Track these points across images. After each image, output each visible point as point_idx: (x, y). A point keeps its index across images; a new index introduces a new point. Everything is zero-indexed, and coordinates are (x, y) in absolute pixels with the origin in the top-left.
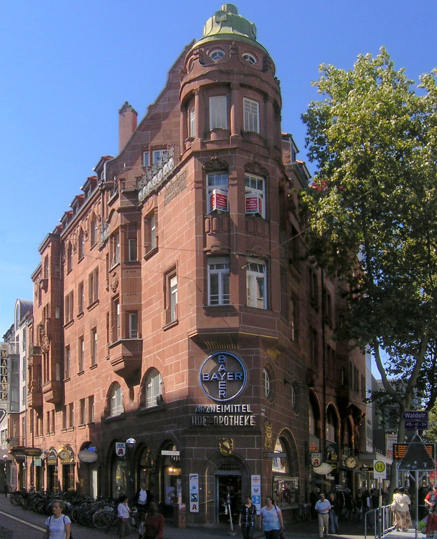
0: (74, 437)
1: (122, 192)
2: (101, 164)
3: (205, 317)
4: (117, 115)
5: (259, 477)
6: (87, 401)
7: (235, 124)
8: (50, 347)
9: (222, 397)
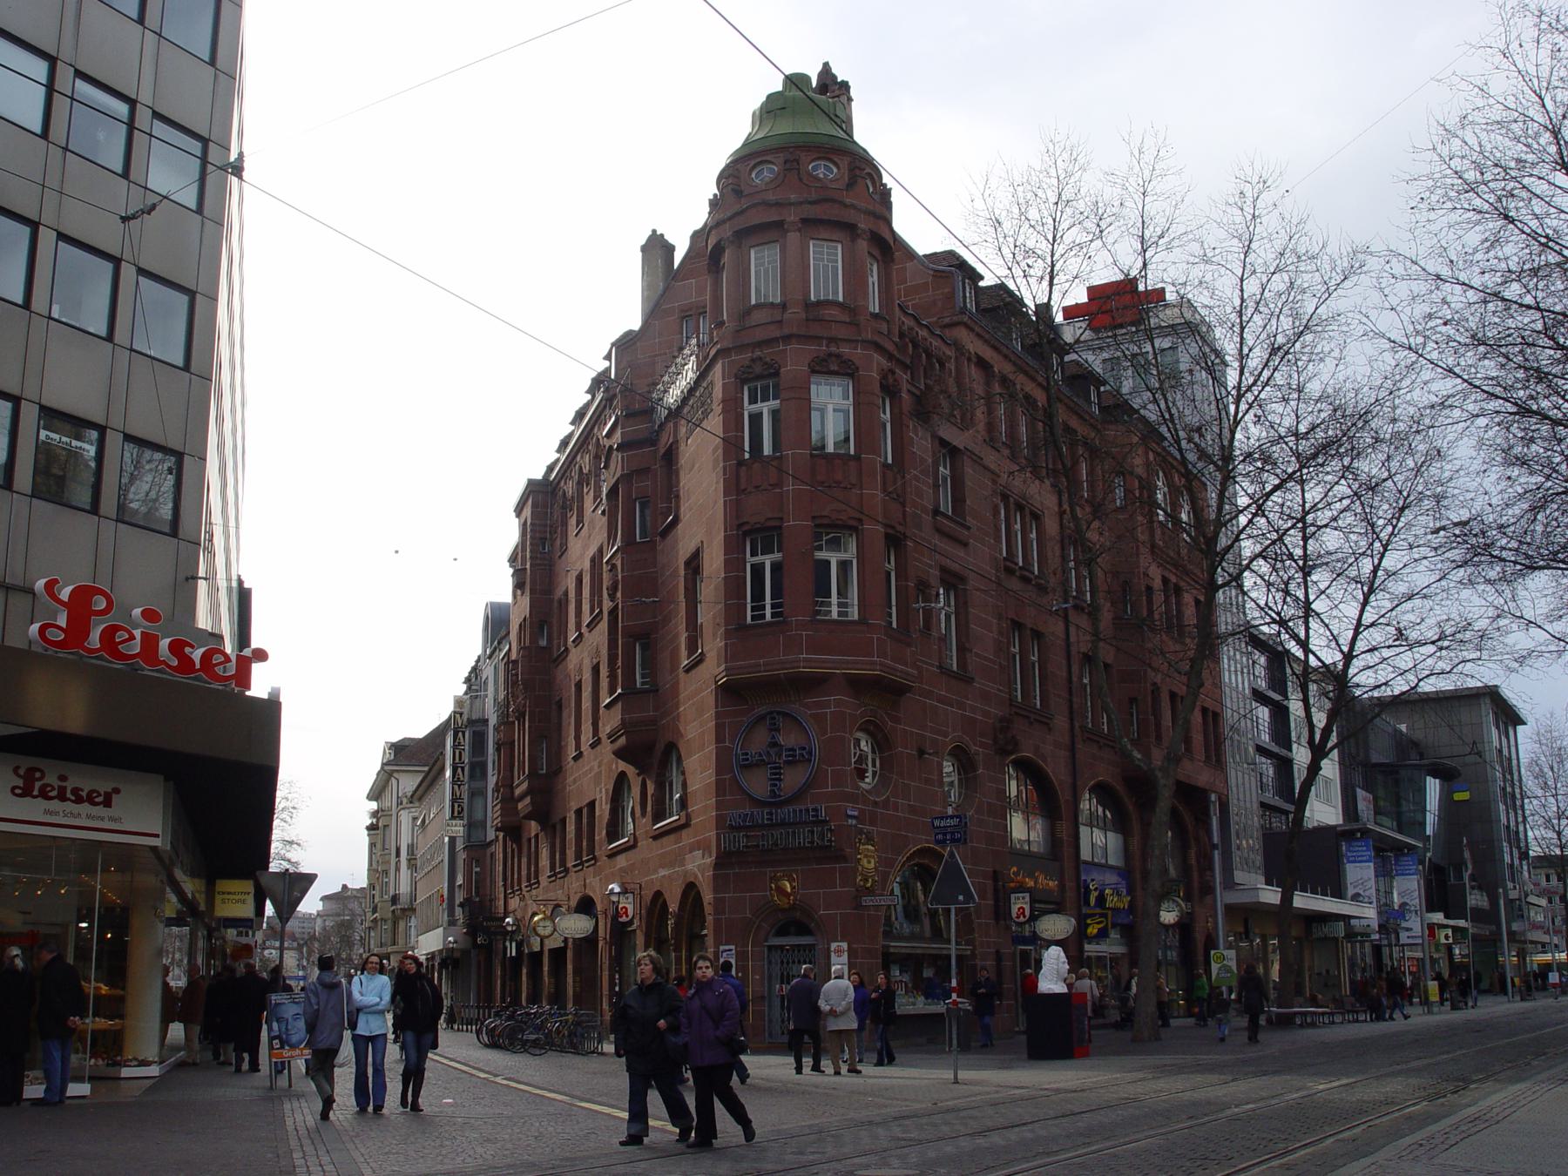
5: (845, 945)
6: (585, 811)
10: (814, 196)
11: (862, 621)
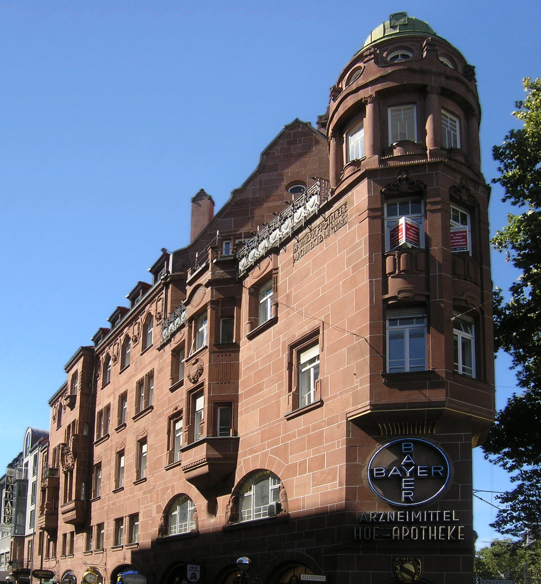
0: (104, 559)
1: (215, 261)
2: (162, 261)
3: (385, 388)
4: (189, 205)
6: (126, 521)
8: (75, 465)
9: (407, 500)
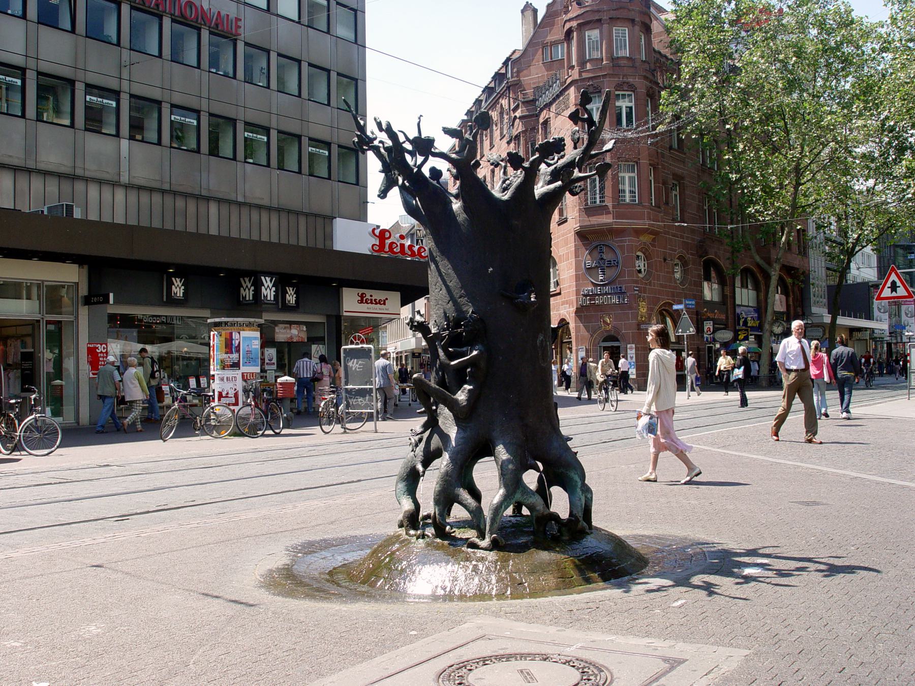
5: (634, 346)
7: (606, 53)
10: (615, 7)
11: (640, 203)
